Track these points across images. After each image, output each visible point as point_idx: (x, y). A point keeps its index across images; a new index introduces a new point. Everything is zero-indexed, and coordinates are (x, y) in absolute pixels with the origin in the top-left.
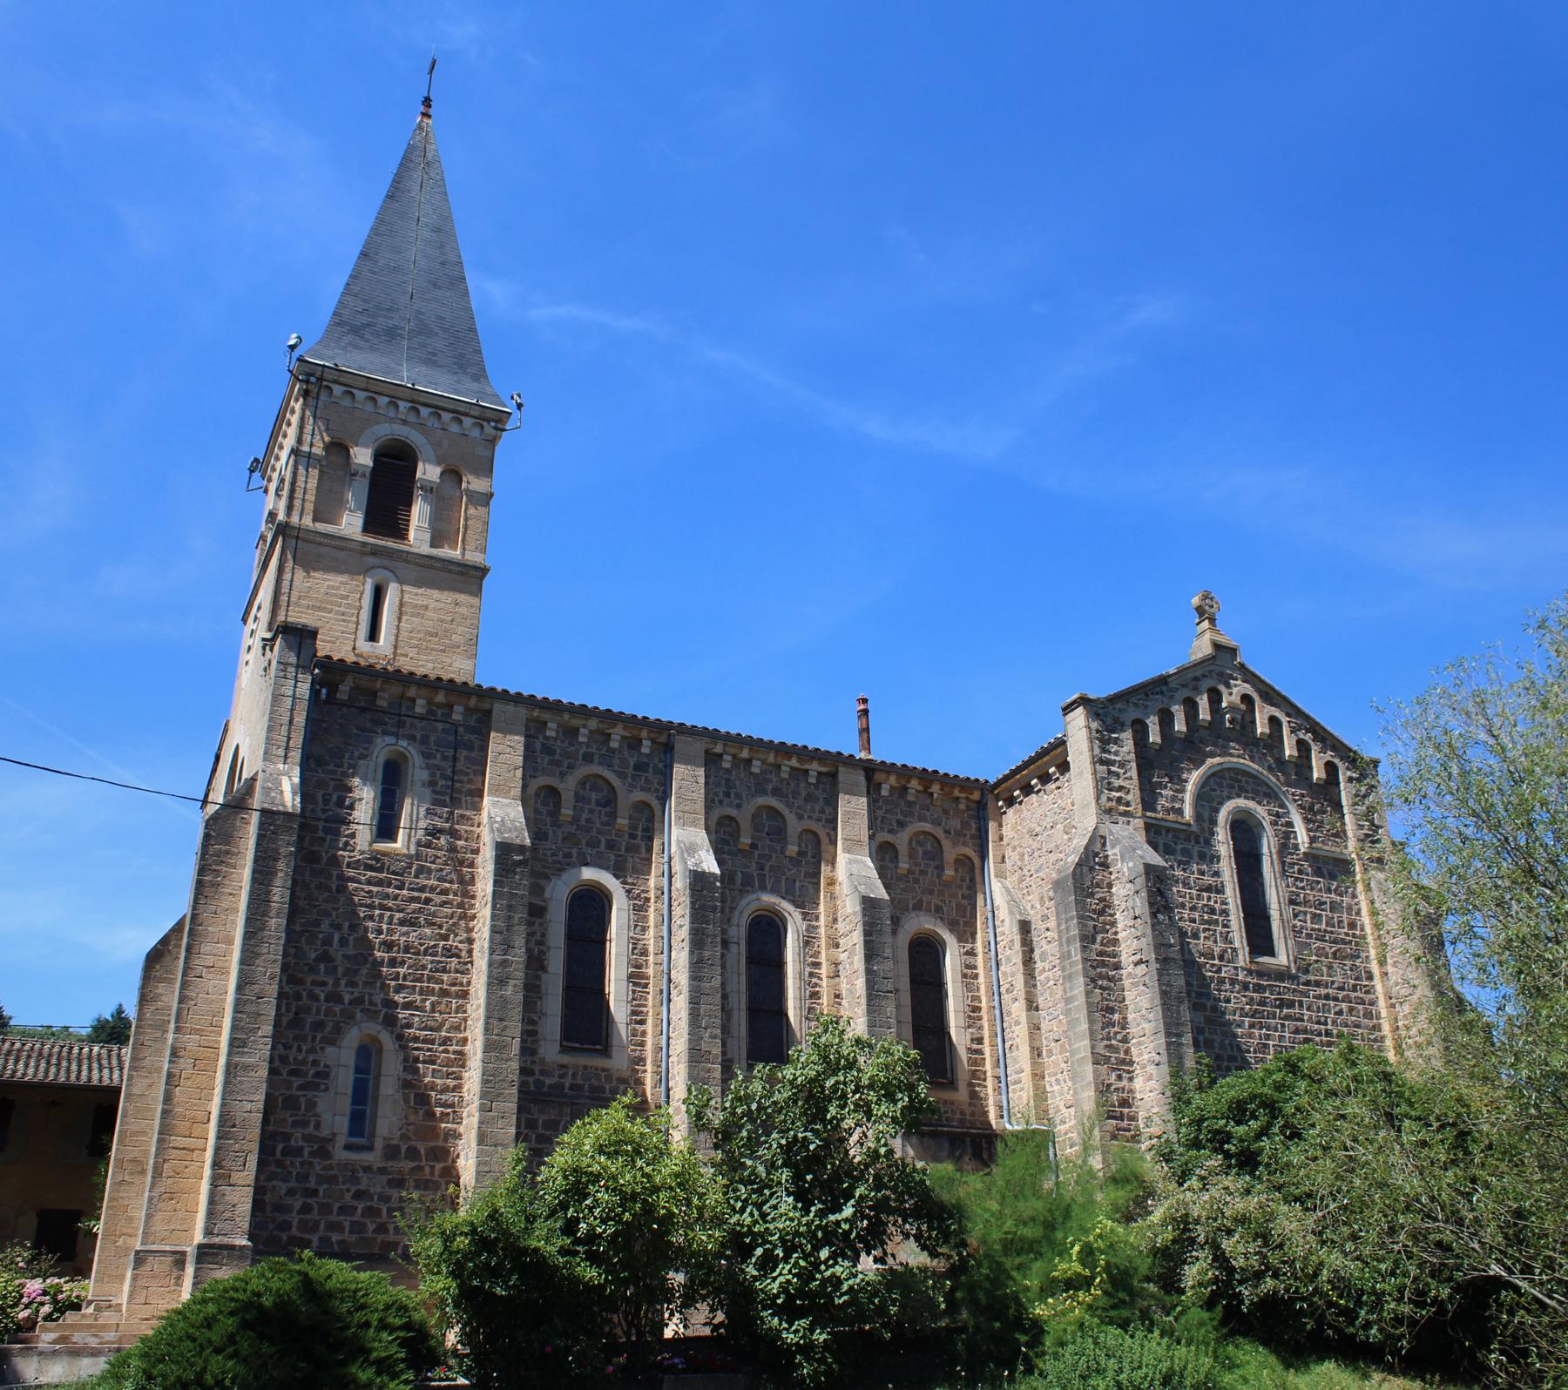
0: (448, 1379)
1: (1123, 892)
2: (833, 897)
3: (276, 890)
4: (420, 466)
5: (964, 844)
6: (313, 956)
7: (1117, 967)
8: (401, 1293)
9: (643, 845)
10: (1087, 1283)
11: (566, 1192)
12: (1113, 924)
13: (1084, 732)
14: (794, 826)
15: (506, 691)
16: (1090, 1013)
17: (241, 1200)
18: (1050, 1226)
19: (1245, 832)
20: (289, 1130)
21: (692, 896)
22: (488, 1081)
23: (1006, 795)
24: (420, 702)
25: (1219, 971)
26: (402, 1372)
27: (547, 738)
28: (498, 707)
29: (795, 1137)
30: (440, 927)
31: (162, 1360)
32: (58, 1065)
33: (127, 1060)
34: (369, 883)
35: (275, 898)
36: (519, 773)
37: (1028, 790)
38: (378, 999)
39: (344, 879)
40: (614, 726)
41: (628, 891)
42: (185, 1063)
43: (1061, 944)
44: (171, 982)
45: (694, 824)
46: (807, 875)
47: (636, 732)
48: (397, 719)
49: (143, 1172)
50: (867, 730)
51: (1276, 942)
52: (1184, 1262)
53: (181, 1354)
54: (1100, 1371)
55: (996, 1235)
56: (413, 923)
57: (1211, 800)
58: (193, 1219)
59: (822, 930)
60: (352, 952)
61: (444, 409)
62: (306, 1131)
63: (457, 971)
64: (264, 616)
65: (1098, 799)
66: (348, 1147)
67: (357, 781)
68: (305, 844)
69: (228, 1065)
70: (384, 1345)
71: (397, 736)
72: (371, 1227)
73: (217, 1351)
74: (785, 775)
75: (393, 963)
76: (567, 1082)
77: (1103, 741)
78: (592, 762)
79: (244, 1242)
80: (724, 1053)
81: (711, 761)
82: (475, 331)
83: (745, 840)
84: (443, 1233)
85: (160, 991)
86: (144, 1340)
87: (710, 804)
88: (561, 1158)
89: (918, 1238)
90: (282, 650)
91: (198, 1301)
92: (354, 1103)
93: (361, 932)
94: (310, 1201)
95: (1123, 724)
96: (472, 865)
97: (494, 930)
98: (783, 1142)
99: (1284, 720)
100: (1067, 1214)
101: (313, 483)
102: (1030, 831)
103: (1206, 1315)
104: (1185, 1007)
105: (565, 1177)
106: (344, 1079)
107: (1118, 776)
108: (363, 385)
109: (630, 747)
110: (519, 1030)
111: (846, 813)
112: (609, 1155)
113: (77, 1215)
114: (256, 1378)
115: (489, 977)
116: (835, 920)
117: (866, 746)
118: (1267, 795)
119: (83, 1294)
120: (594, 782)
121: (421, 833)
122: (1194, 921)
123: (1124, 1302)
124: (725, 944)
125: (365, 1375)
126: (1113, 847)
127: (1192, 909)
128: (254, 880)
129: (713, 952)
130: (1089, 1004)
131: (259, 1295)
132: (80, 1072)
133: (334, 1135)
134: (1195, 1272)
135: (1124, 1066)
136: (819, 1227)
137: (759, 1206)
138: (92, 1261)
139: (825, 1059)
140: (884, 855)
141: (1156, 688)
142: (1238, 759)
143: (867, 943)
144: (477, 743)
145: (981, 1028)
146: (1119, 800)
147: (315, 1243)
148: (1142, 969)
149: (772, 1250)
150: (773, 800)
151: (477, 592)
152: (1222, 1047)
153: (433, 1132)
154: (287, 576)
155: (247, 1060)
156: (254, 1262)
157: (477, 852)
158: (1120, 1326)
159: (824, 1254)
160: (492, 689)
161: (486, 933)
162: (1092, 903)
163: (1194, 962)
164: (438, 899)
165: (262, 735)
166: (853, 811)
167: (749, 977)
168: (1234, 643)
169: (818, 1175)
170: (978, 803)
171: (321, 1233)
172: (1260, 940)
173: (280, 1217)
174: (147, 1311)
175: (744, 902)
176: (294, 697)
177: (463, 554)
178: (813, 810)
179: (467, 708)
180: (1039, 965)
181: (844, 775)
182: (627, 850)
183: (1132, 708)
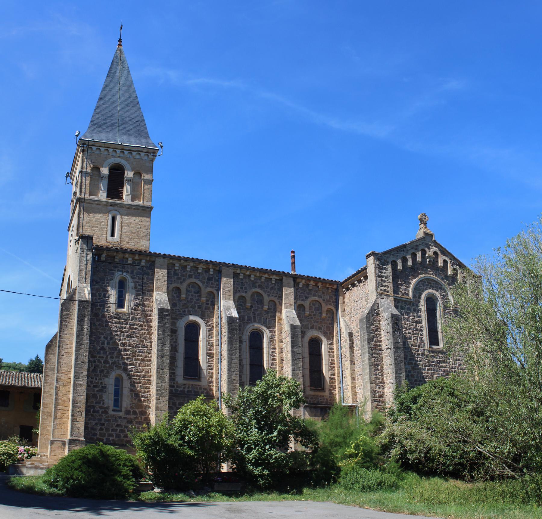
1: (384, 324)
2: (281, 325)
4: (126, 172)
5: (330, 304)
6: (99, 348)
7: (381, 350)
8: (130, 456)
11: (181, 427)
12: (380, 335)
13: (373, 266)
14: (266, 299)
15: (160, 254)
16: (370, 366)
17: (81, 426)
18: (345, 438)
19: (431, 302)
20: (95, 405)
21: (228, 325)
22: (158, 390)
23: (352, 282)
24: (130, 259)
25: (418, 351)
26: (131, 479)
27: (175, 270)
28: (157, 260)
29: (258, 410)
31: (61, 471)
32: (22, 380)
33: (43, 379)
34: (116, 323)
36: (166, 283)
37: (353, 285)
38: (121, 362)
39: (107, 322)
40: (199, 264)
41: (206, 324)
42: (61, 383)
44: (54, 355)
45: (229, 299)
46: (271, 316)
48: (122, 265)
49: (51, 416)
54: (358, 482)
55: (327, 440)
56: (131, 337)
58: (67, 431)
59: (277, 336)
60: (111, 347)
62: (100, 405)
63: (147, 353)
64: (75, 229)
65: (377, 290)
66: (114, 410)
67: (109, 288)
68: (94, 311)
69: (74, 384)
70: (125, 471)
71: (122, 271)
72: (122, 436)
73: (76, 470)
74: (263, 280)
75: (125, 350)
76: (186, 390)
77: (380, 268)
79: (83, 439)
80: (240, 380)
81: (235, 276)
82: (144, 120)
83: (248, 305)
84: (141, 438)
86: (55, 465)
87: (235, 292)
88: (179, 416)
89: (301, 442)
91: (70, 455)
92: (115, 396)
93: (114, 340)
95: (388, 262)
96: (150, 316)
97: (159, 339)
98: (254, 411)
99: (449, 261)
100: (352, 434)
101: (88, 182)
103: (396, 464)
104: (403, 364)
105: (181, 422)
106: (111, 389)
107: (385, 281)
108: (103, 146)
109: (206, 272)
110: (168, 373)
111: (286, 294)
112: (195, 416)
113: (31, 428)
114: (88, 478)
116: (281, 333)
117: (294, 269)
118: (441, 288)
120: (193, 285)
121: (132, 305)
122: (410, 333)
123: (368, 461)
124: (241, 341)
125: (120, 479)
126: (381, 307)
127: (409, 329)
128: (78, 324)
129: (236, 345)
130: (370, 363)
131: (87, 455)
132: (28, 382)
133: (109, 406)
134: (395, 452)
135: (381, 384)
136: (266, 439)
137: (246, 432)
138: (38, 442)
139: (268, 384)
140: (300, 309)
141: (402, 248)
142: (431, 275)
145: (334, 370)
146: (385, 290)
147: (105, 440)
150: (259, 290)
151: (149, 216)
153: (141, 406)
154: (82, 216)
155: (80, 383)
156: (86, 445)
157: (152, 311)
158: (366, 468)
159: (267, 447)
160: (155, 253)
161: (156, 340)
162: (373, 327)
164: (139, 328)
166: (288, 293)
168: (432, 233)
170: (336, 289)
171: (106, 437)
172: (434, 339)
173: (93, 432)
174: (56, 458)
176: (87, 260)
177: (143, 203)
178: (273, 293)
179: (146, 260)
180: (355, 348)
181: (285, 280)
182: (205, 309)
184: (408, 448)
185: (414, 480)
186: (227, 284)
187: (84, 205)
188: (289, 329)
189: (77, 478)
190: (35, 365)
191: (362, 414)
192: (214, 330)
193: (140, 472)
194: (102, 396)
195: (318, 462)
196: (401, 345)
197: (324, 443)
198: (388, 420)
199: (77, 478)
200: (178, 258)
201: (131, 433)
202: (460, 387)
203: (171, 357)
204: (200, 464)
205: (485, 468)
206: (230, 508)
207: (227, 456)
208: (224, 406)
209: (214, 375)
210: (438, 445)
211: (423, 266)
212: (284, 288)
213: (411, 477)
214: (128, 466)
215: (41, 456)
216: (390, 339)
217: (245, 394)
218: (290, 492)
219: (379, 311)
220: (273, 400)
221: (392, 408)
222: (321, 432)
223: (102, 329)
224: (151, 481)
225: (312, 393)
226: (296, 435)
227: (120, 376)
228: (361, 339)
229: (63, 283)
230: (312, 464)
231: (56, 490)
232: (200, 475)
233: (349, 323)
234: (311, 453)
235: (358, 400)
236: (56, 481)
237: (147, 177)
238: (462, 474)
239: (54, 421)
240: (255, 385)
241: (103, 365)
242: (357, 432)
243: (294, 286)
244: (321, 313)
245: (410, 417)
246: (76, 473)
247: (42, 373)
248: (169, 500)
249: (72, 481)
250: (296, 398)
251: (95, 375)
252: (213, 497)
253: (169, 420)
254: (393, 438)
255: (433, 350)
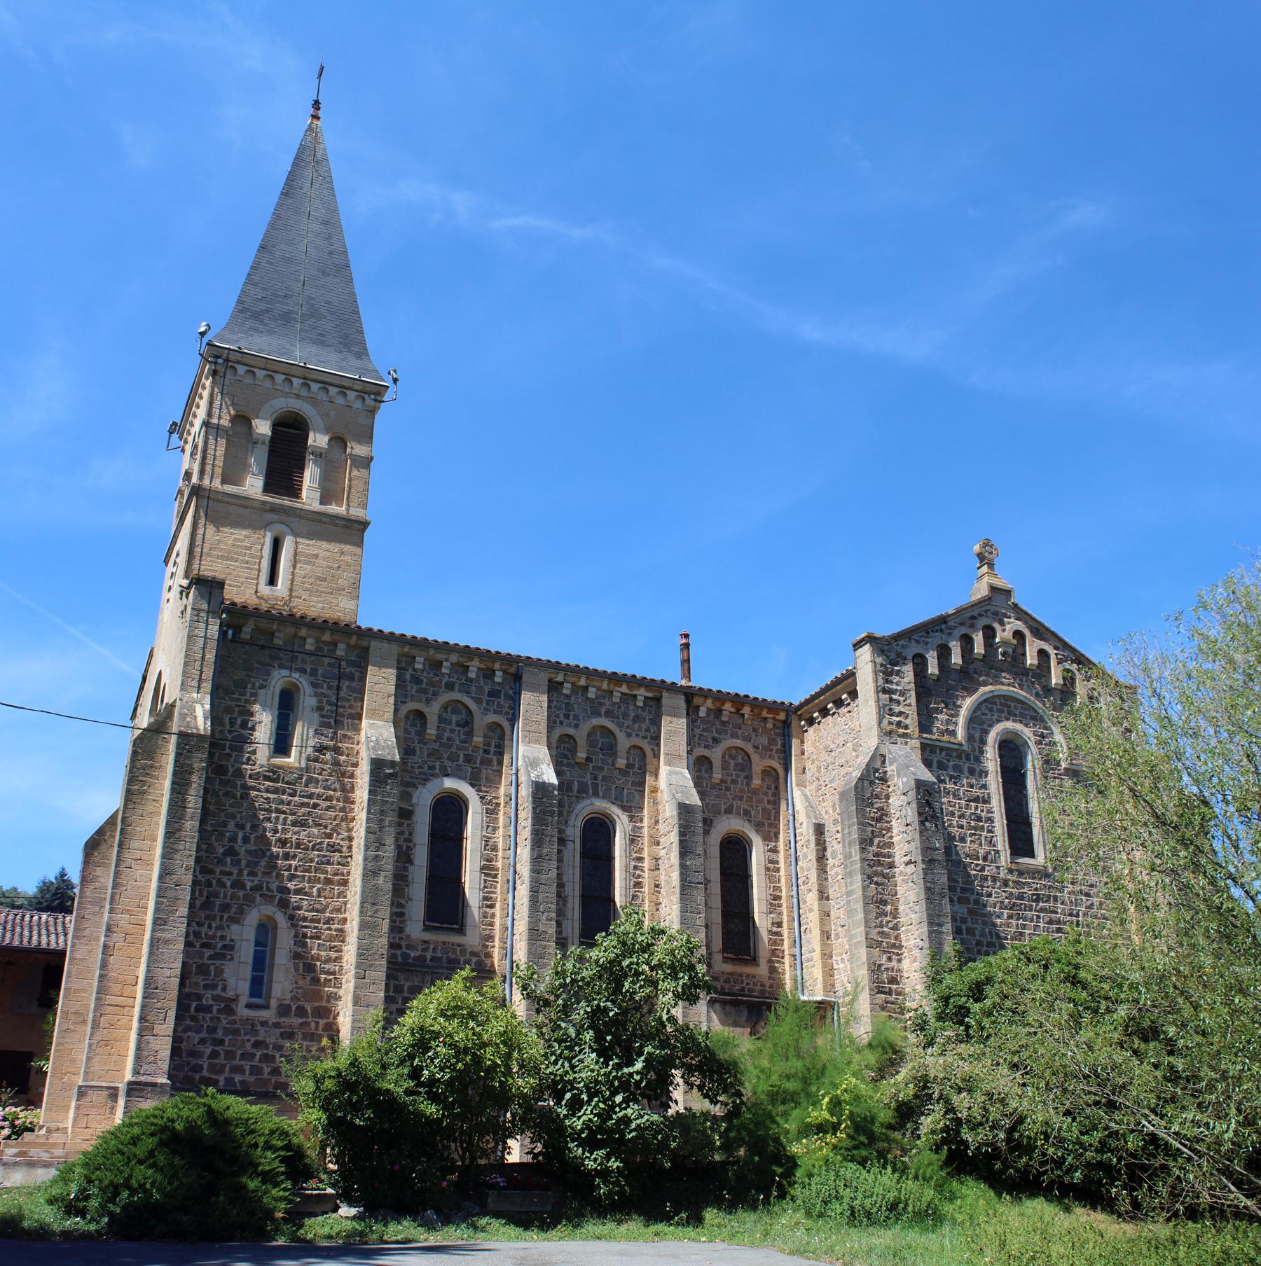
0: (318, 1189)
1: (898, 803)
2: (655, 803)
3: (191, 798)
4: (311, 435)
5: (771, 757)
6: (221, 851)
7: (891, 866)
9: (495, 758)
10: (835, 1128)
11: (413, 1046)
12: (889, 829)
13: (870, 667)
14: (623, 742)
15: (381, 631)
16: (866, 905)
17: (162, 1047)
18: (806, 1081)
19: (1011, 752)
20: (202, 992)
21: (534, 802)
23: (821, 706)
24: (309, 640)
25: (983, 869)
26: (282, 1182)
27: (415, 670)
28: (375, 645)
29: (598, 1005)
30: (326, 827)
32: (13, 930)
33: (71, 928)
34: (267, 791)
35: (191, 805)
36: (392, 700)
37: (825, 712)
38: (274, 886)
39: (246, 788)
40: (472, 660)
41: (482, 798)
43: (844, 847)
44: (106, 866)
45: (538, 742)
47: (490, 665)
48: (289, 655)
49: (84, 1022)
50: (688, 661)
51: (1035, 846)
52: (923, 1114)
53: (113, 1164)
55: (763, 1087)
57: (982, 723)
58: (124, 1062)
59: (646, 830)
60: (253, 848)
61: (331, 384)
62: (215, 993)
63: (339, 864)
65: (880, 723)
66: (249, 1006)
67: (257, 707)
68: (216, 759)
70: (269, 1161)
71: (291, 669)
72: (267, 1070)
73: (140, 1162)
75: (287, 856)
77: (886, 672)
78: (453, 689)
79: (165, 1081)
80: (559, 932)
81: (553, 688)
82: (357, 313)
83: (581, 755)
84: (315, 1076)
85: (98, 873)
86: (84, 1154)
88: (410, 1019)
89: (700, 1088)
90: (195, 598)
92: (254, 970)
93: (261, 832)
94: (218, 1048)
95: (905, 659)
96: (352, 776)
97: (369, 831)
98: (589, 1009)
99: (1052, 652)
100: (823, 1071)
101: (221, 451)
102: (826, 748)
104: (946, 901)
105: (413, 1034)
106: (246, 951)
107: (898, 703)
108: (263, 365)
109: (485, 677)
112: (448, 1018)
113: (30, 1056)
114: (170, 1183)
115: (365, 869)
116: (657, 822)
117: (687, 674)
119: (35, 1120)
120: (456, 706)
122: (962, 827)
123: (863, 1144)
124: (562, 841)
125: (253, 1184)
126: (891, 764)
127: (960, 817)
128: (173, 790)
129: (550, 849)
130: (865, 897)
131: (173, 1121)
132: (31, 937)
133: (238, 996)
134: (931, 1121)
135: (894, 949)
136: (616, 1077)
137: (570, 1059)
138: (42, 1094)
139: (624, 944)
140: (700, 767)
141: (938, 625)
142: (1008, 687)
143: (681, 842)
144: (357, 675)
145: (780, 914)
147: (222, 1083)
148: (911, 868)
149: (579, 1095)
150: (606, 720)
151: (359, 543)
152: (983, 934)
153: (317, 995)
154: (200, 531)
155: (167, 935)
156: (172, 1095)
157: (356, 765)
158: (859, 1163)
159: (619, 1099)
160: (370, 630)
161: (362, 832)
162: (872, 812)
163: (960, 862)
164: (324, 804)
165: (181, 659)
166: (674, 730)
167: (583, 870)
168: (1009, 586)
169: (619, 1032)
171: (227, 1074)
172: (1021, 842)
173: (193, 1061)
174: (87, 1134)
175: (580, 806)
176: (205, 637)
177: (348, 510)
178: (640, 729)
179: (348, 646)
180: (830, 862)
181: (667, 699)
183: (913, 643)
184: (963, 1115)
185: (982, 1202)
186: (533, 705)
187: (207, 504)
188: (675, 813)
189: (142, 1186)
190: (55, 894)
191: (847, 1022)
192: (501, 813)
193: (305, 1165)
194: (222, 971)
195: (740, 1141)
196: (940, 855)
197: (755, 1093)
198: (912, 1038)
199: (142, 1186)
200: (423, 644)
201: (289, 1061)
202: (1093, 962)
203: (396, 876)
204: (455, 1141)
205: (1170, 1180)
206: (524, 1258)
207: (523, 1120)
208: (517, 996)
209: (497, 921)
210: (1041, 1113)
211: (989, 666)
212: (664, 718)
213: (973, 1192)
214: (275, 1149)
215: (49, 1131)
216: (913, 840)
217: (569, 966)
218: (673, 1218)
219: (885, 772)
220: (633, 983)
221: (921, 1011)
222: (747, 1065)
223: (232, 806)
224: (333, 1186)
225: (728, 968)
226: (689, 1070)
227: (271, 919)
228: (843, 839)
229: (142, 688)
230: (727, 1147)
231: (82, 1222)
232: (452, 1169)
233: (815, 802)
234: (723, 1119)
235: (838, 987)
236: (83, 1196)
237: (358, 450)
238: (1109, 1192)
239: (92, 1035)
240: (593, 945)
241: (230, 891)
242: (835, 1067)
243: (688, 714)
244: (749, 778)
245: (968, 1035)
246: (142, 1173)
247: (71, 913)
248: (375, 1237)
249: (126, 1194)
250: (690, 978)
251: (207, 917)
252: (483, 1230)
253: (384, 1028)
254: (925, 1087)
255: (1020, 867)
